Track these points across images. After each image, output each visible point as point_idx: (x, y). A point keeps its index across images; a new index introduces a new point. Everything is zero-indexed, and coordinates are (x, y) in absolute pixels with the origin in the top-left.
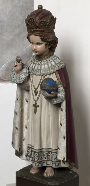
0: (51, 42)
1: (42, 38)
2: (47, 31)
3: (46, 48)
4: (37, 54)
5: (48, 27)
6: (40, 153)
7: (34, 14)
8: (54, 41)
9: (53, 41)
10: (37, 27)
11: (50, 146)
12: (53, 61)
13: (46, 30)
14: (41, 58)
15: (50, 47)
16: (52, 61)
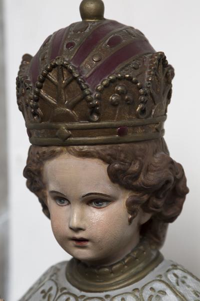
0: (155, 191)
1: (117, 170)
2: (140, 133)
3: (130, 221)
4: (85, 253)
5: (143, 111)
6: (53, 278)
7: (70, 45)
8: (170, 186)
9: (168, 182)
10: (93, 110)
11: (46, 92)
12: (168, 291)
13: (135, 126)
14: (105, 277)
15: (146, 218)
16: (164, 293)
